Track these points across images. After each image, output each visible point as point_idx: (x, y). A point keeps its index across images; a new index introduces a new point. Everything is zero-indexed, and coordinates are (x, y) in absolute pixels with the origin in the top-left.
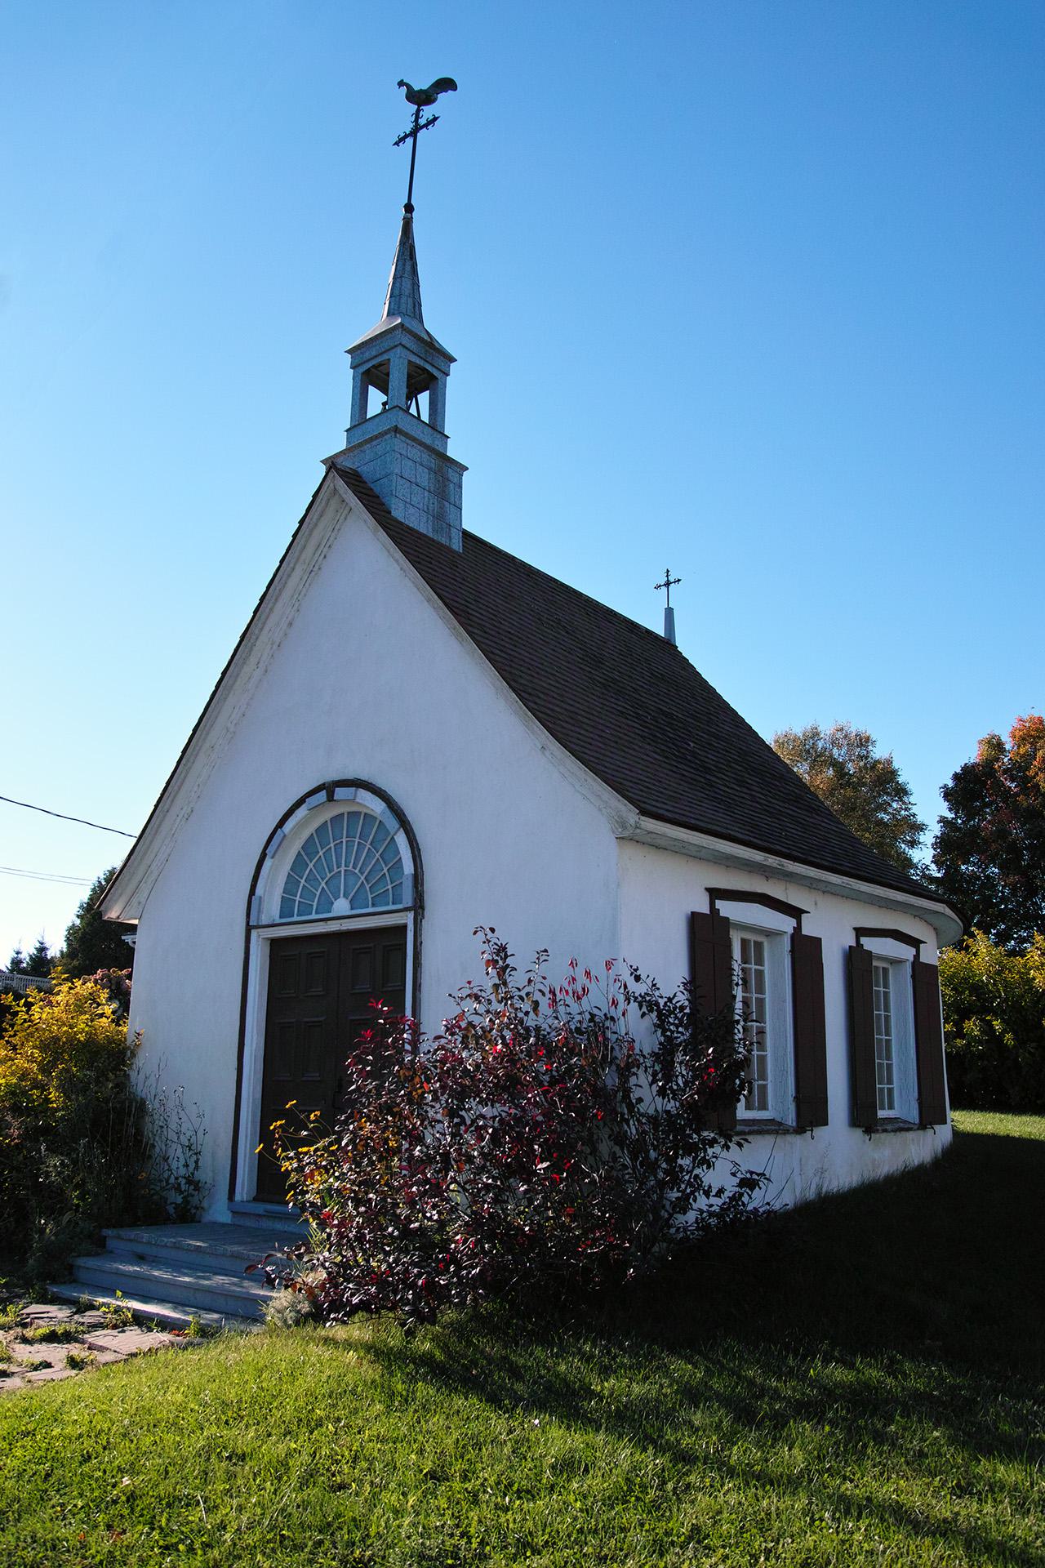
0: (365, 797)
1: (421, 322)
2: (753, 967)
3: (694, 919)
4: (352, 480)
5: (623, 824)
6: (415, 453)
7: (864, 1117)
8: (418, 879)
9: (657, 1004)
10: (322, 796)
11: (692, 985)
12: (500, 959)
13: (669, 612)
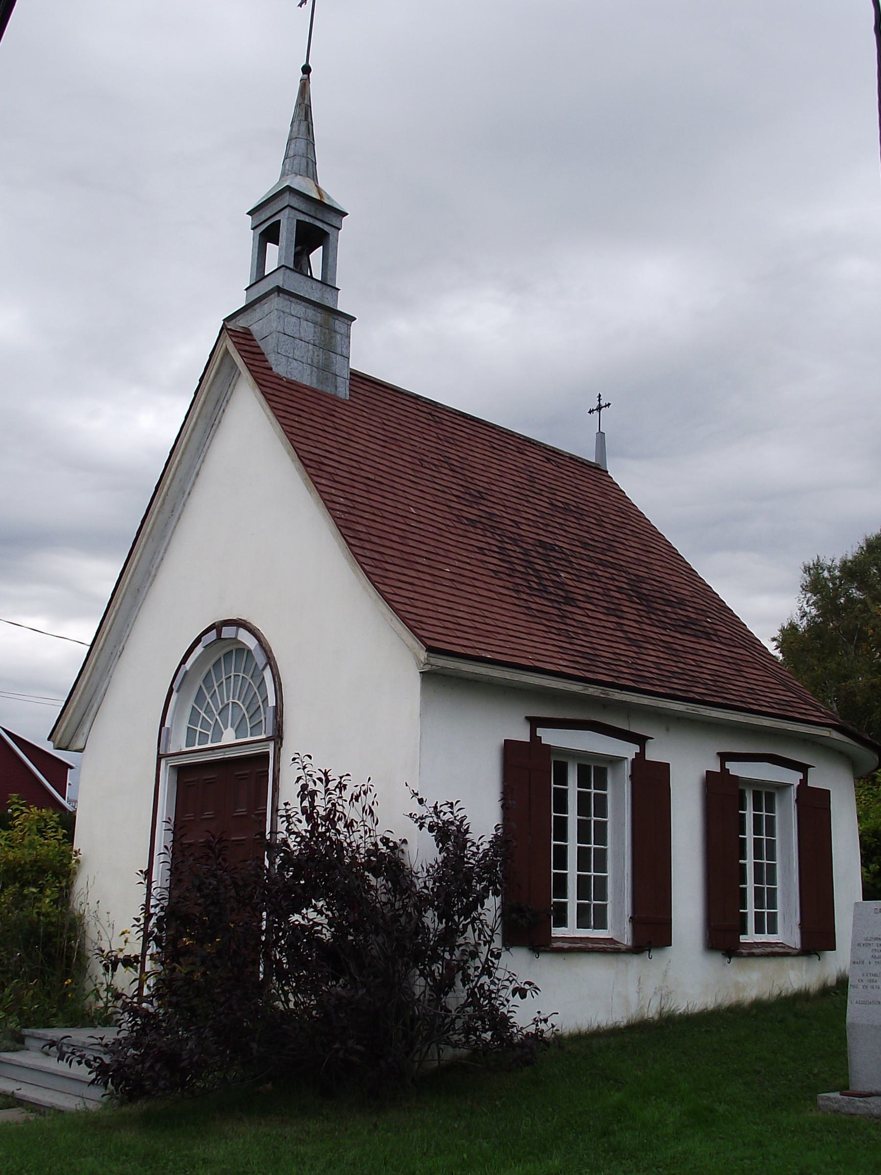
0: (245, 637)
1: (314, 178)
3: (510, 749)
4: (240, 345)
8: (278, 711)
10: (213, 635)
13: (601, 435)
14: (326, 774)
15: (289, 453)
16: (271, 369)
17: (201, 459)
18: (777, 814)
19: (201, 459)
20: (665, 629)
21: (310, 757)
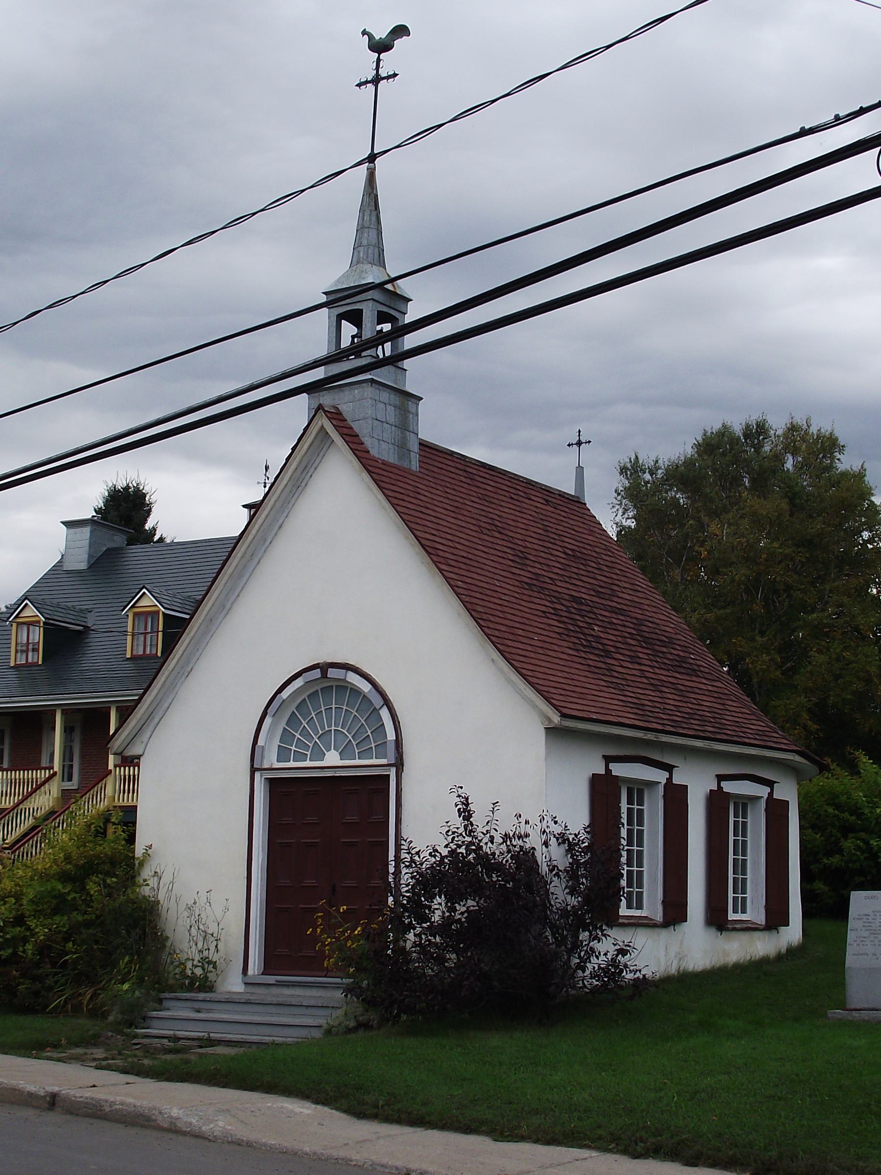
2: (636, 807)
5: (550, 720)
6: (385, 395)
7: (717, 919)
9: (568, 839)
10: (317, 673)
11: (593, 827)
12: (466, 813)
13: (580, 470)
14: (467, 799)
15: (407, 538)
16: (368, 452)
17: (285, 514)
18: (749, 820)
19: (285, 514)
20: (668, 670)
21: (461, 788)
